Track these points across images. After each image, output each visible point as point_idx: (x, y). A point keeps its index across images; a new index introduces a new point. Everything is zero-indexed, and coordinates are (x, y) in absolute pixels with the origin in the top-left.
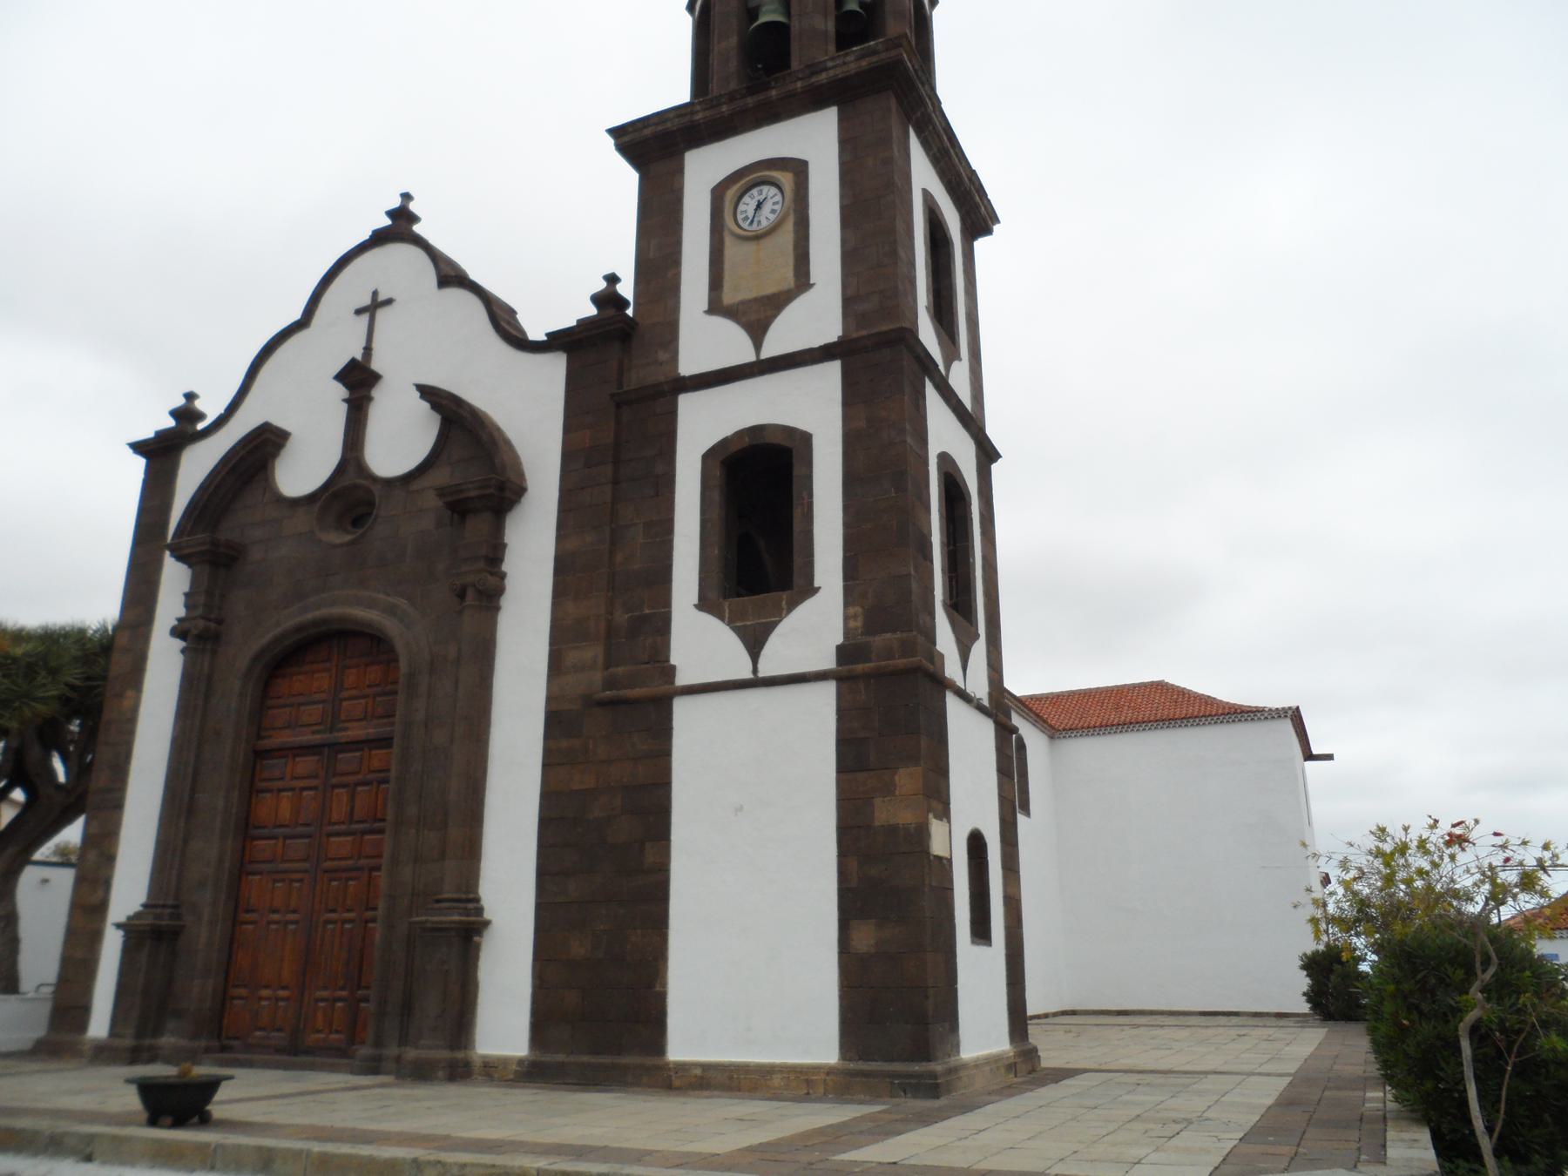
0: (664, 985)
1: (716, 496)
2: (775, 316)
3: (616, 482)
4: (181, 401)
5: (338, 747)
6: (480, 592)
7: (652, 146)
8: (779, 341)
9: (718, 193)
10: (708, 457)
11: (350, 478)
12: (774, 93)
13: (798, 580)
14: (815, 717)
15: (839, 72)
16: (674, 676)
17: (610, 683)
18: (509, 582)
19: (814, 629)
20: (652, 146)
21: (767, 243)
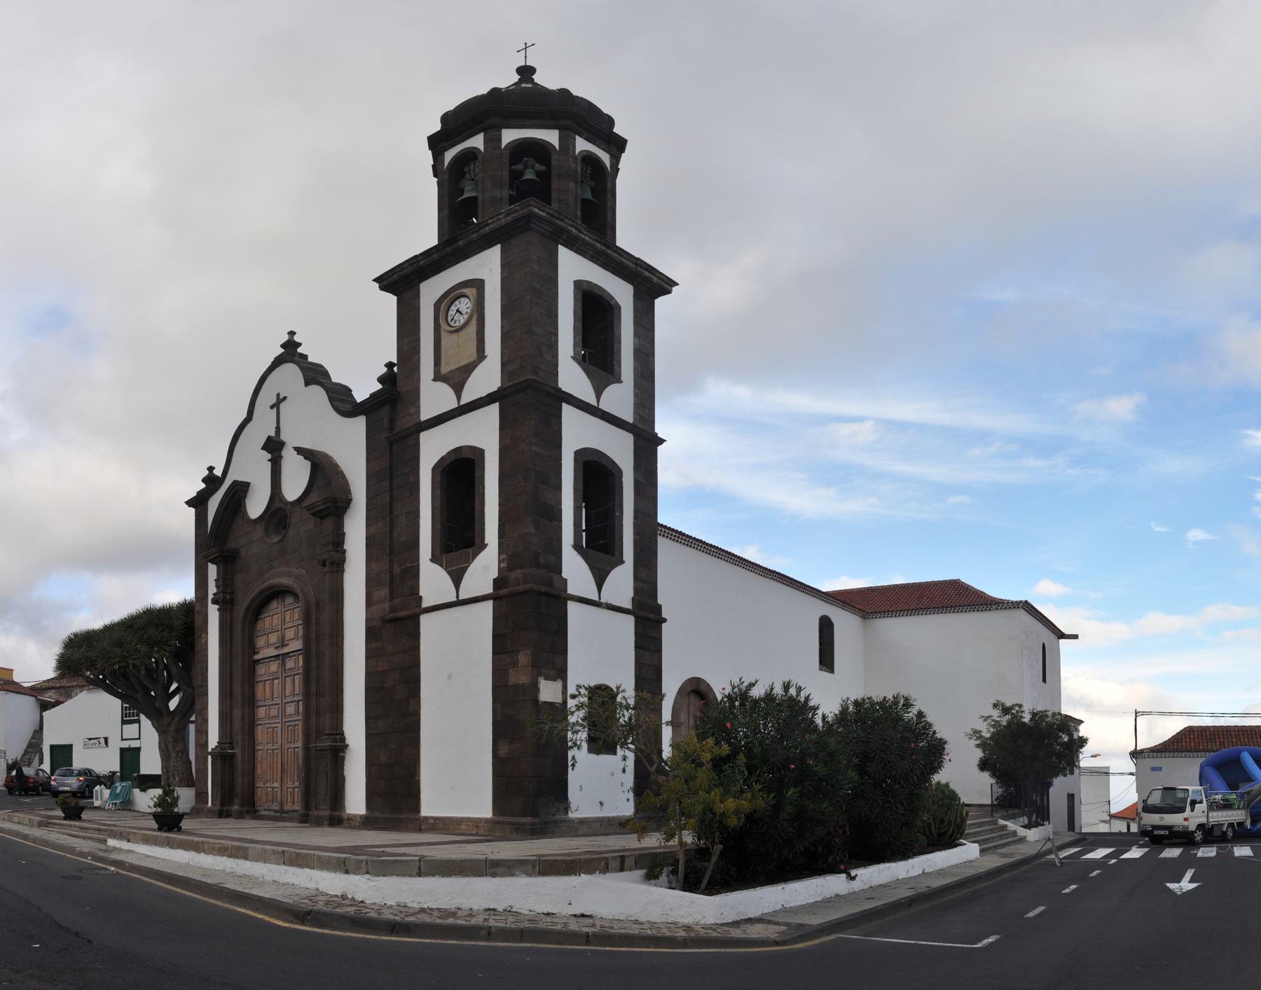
1: (438, 492)
3: (391, 490)
4: (286, 338)
5: (285, 655)
7: (402, 282)
8: (469, 395)
9: (437, 305)
11: (277, 505)
13: (477, 541)
15: (495, 226)
17: (393, 609)
19: (484, 570)
21: (463, 333)
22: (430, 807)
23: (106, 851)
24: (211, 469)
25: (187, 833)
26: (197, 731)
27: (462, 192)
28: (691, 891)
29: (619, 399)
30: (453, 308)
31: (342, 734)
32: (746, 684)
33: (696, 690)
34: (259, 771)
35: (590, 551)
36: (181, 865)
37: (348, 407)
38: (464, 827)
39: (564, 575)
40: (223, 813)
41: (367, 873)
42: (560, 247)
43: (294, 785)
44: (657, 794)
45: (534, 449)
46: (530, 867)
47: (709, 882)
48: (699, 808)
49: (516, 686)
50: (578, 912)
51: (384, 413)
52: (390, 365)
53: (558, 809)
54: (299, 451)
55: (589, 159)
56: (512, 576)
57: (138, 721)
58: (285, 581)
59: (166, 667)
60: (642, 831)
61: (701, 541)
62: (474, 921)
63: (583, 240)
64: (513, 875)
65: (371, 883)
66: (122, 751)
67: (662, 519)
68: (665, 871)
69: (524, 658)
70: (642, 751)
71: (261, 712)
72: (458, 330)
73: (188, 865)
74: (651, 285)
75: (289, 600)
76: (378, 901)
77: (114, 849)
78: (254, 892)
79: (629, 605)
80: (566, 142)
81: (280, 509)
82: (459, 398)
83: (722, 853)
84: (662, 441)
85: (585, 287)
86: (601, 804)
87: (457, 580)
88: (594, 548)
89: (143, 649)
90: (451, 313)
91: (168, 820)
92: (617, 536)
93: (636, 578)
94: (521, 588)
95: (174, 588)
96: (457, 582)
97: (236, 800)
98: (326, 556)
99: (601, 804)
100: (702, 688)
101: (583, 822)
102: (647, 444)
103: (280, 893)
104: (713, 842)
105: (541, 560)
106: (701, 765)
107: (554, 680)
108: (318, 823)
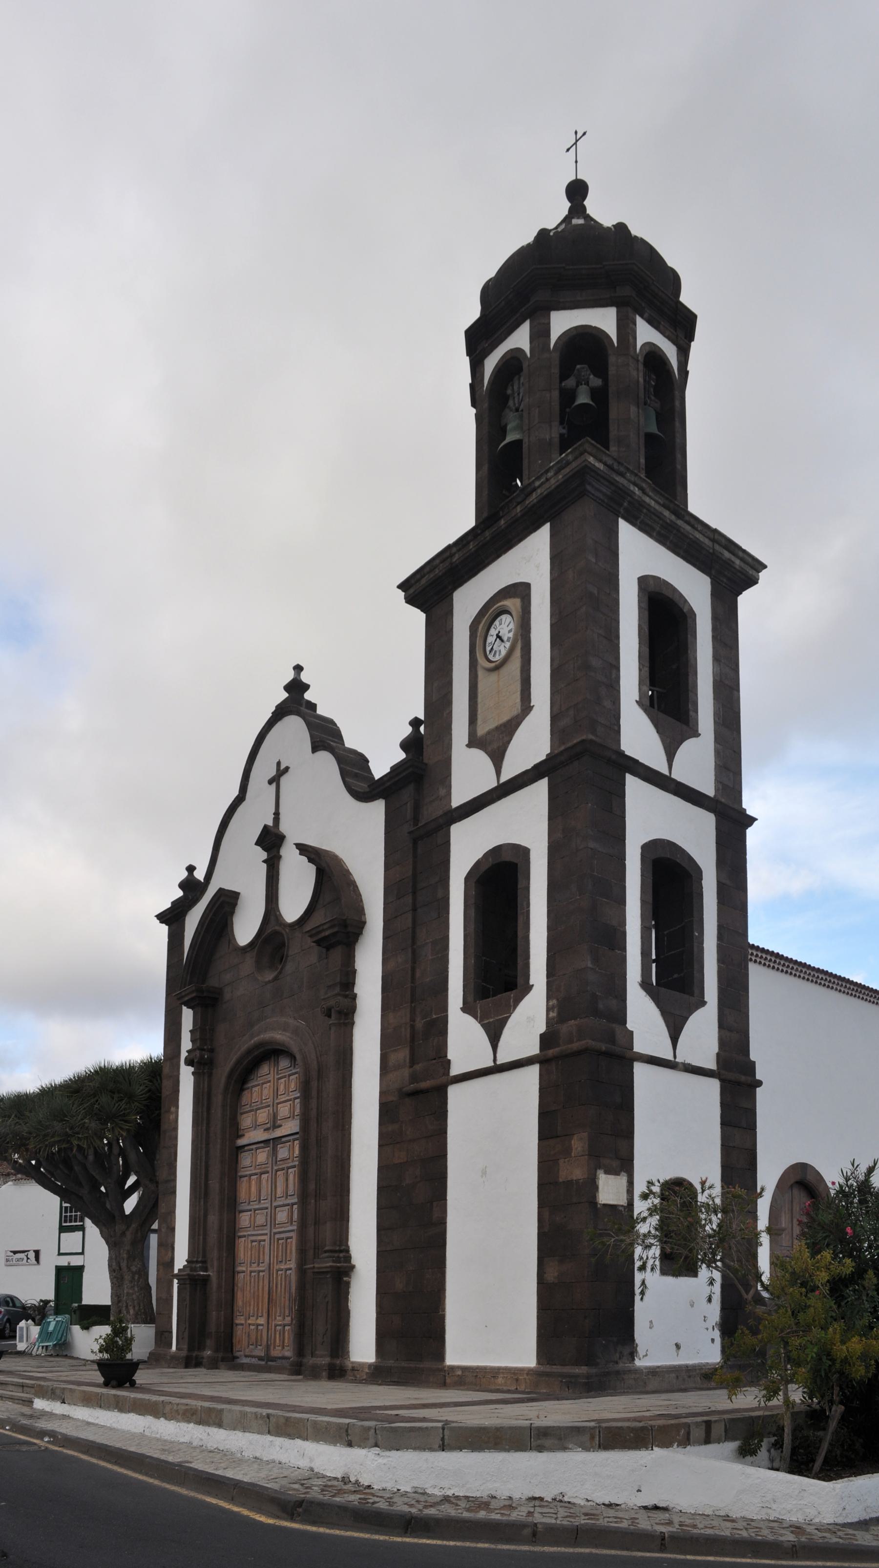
2: (509, 742)
3: (415, 910)
4: (290, 676)
5: (277, 1140)
6: (340, 1012)
7: (431, 588)
8: (513, 767)
11: (272, 927)
12: (502, 522)
13: (520, 981)
17: (414, 1078)
18: (359, 1002)
21: (504, 671)
22: (456, 1355)
23: (31, 1417)
24: (191, 869)
25: (143, 1389)
26: (160, 1245)
27: (503, 432)
28: (800, 1473)
29: (696, 763)
30: (493, 632)
31: (347, 1250)
32: (863, 1169)
33: (801, 1181)
34: (239, 1302)
35: (663, 990)
36: (133, 1436)
37: (363, 786)
38: (500, 1380)
39: (629, 1026)
40: (191, 1362)
41: (376, 1445)
42: (624, 527)
43: (284, 1320)
44: (755, 1332)
45: (592, 845)
46: (586, 1438)
47: (826, 1462)
48: (812, 1352)
49: (569, 1184)
50: (650, 1502)
51: (407, 795)
52: (415, 723)
53: (621, 1356)
54: (303, 849)
55: (654, 356)
56: (564, 1029)
57: (82, 1228)
58: (279, 1036)
59: (122, 1152)
60: (733, 1386)
61: (804, 965)
62: (515, 1516)
63: (648, 507)
64: (564, 1449)
65: (381, 1460)
66: (59, 1270)
67: (753, 938)
68: (766, 1443)
69: (578, 1144)
70: (735, 1271)
71: (244, 1219)
72: (498, 667)
73: (142, 1435)
74: (732, 570)
75: (284, 1063)
76: (389, 1486)
77: (43, 1414)
78: (230, 1474)
79: (712, 1065)
80: (626, 328)
81: (276, 933)
82: (498, 773)
83: (843, 1418)
84: (751, 820)
86: (678, 1346)
88: (668, 986)
89: (93, 1125)
90: (491, 639)
91: (117, 1371)
92: (696, 966)
93: (722, 1025)
94: (576, 1046)
95: (138, 1042)
96: (494, 1039)
97: (209, 1342)
98: (332, 1003)
99: (678, 1346)
100: (810, 1178)
101: (654, 1372)
102: (732, 824)
103: (263, 1474)
104: (831, 1402)
105: (601, 1006)
106: (814, 1289)
107: (619, 1175)
108: (314, 1374)
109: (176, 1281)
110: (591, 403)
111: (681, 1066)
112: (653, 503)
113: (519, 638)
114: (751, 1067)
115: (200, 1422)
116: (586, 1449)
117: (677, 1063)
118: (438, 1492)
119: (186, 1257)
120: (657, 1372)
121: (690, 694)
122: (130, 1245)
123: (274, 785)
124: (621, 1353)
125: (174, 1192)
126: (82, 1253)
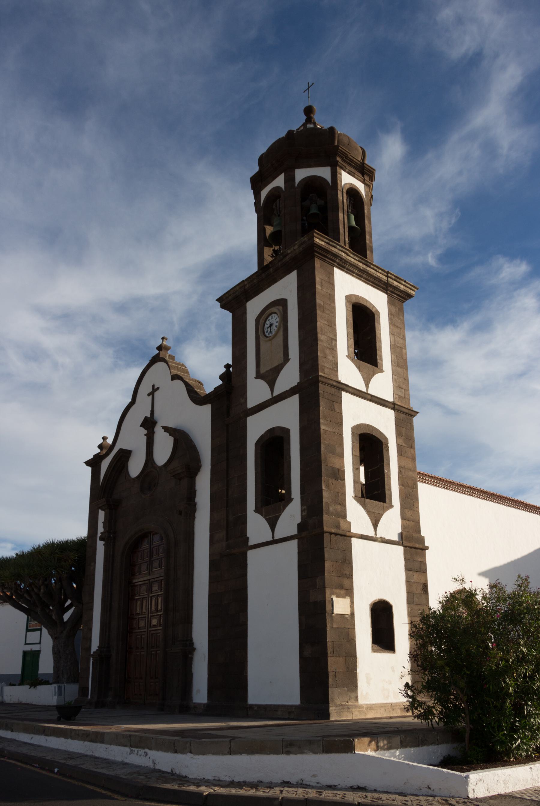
0: (247, 673)
4: (160, 342)
7: (234, 301)
9: (258, 320)
10: (257, 444)
12: (271, 270)
14: (290, 551)
16: (248, 541)
19: (291, 517)
20: (234, 301)
29: (383, 384)
31: (191, 640)
39: (348, 519)
52: (227, 366)
55: (353, 192)
57: (40, 630)
64: (302, 753)
66: (25, 653)
72: (271, 339)
82: (272, 391)
85: (354, 300)
87: (273, 526)
93: (403, 517)
96: (273, 526)
105: (331, 509)
107: (344, 598)
109: (92, 659)
110: (318, 212)
111: (379, 539)
112: (353, 260)
113: (282, 325)
114: (422, 540)
115: (91, 741)
116: (315, 753)
117: (377, 538)
118: (227, 779)
119: (98, 645)
120: (373, 708)
121: (378, 352)
122: (68, 638)
123: (151, 396)
124: (350, 696)
125: (92, 609)
126: (40, 643)
